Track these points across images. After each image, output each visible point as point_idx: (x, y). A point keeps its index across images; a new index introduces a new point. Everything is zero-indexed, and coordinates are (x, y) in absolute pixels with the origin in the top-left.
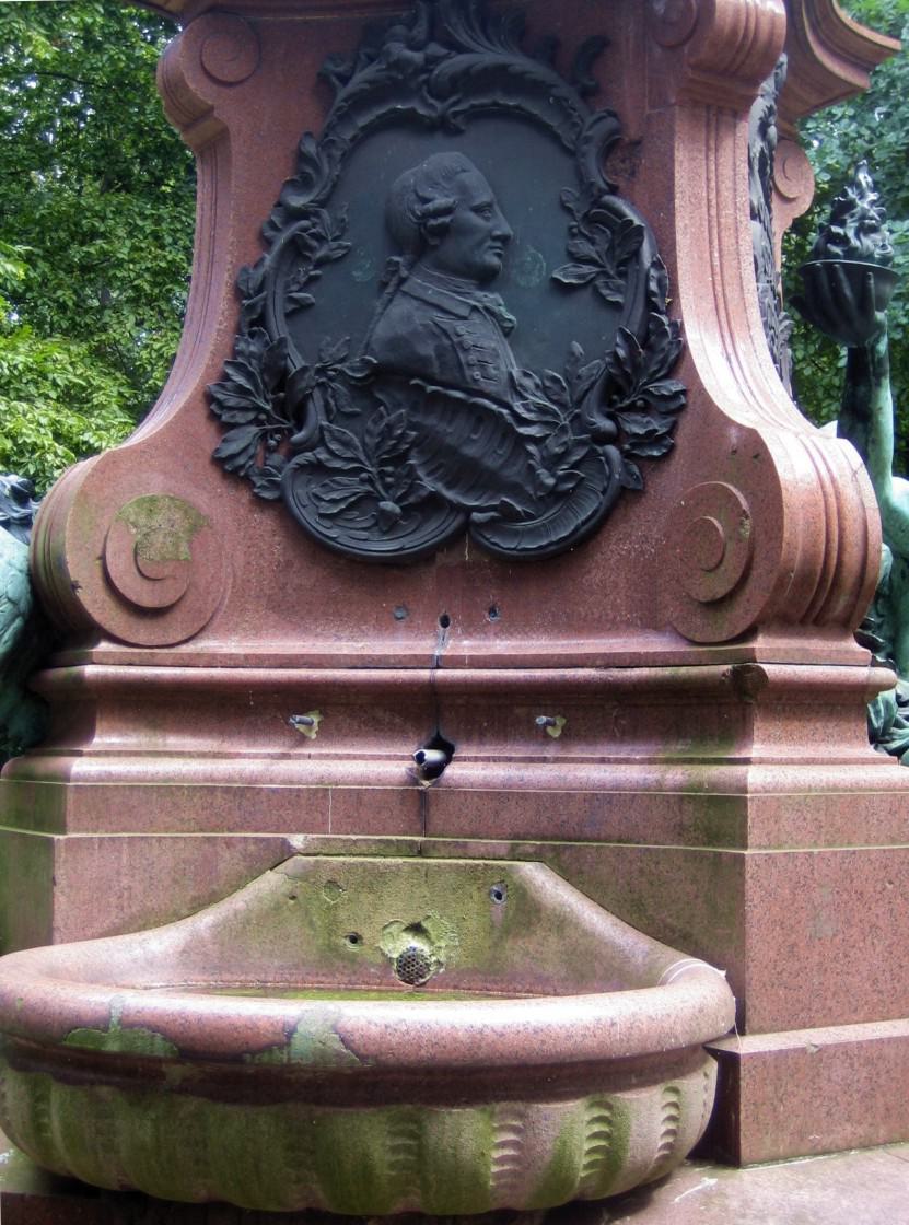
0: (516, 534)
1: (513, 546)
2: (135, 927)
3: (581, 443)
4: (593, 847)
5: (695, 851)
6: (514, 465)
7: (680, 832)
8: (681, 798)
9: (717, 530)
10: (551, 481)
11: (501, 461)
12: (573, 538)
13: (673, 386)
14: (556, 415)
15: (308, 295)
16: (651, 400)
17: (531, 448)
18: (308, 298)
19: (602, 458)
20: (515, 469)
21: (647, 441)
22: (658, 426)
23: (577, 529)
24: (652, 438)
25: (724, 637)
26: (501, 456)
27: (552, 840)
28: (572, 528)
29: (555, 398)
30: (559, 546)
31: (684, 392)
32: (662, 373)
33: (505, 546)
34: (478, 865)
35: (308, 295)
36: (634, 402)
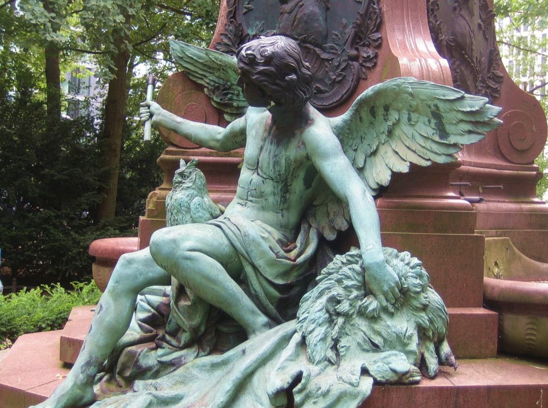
0: (322, 99)
1: (320, 104)
2: (534, 280)
3: (344, 61)
4: (415, 211)
5: (543, 232)
6: (321, 71)
7: (530, 225)
8: (531, 214)
9: (517, 123)
10: (334, 77)
11: (316, 69)
12: (342, 100)
13: (377, 35)
14: (336, 50)
15: (251, 6)
16: (371, 42)
17: (326, 64)
18: (251, 7)
19: (352, 67)
20: (321, 72)
21: (367, 60)
22: (371, 52)
23: (342, 96)
24: (368, 59)
25: (525, 162)
26: (316, 67)
27: (506, 229)
28: (340, 96)
29: (336, 42)
30: (337, 103)
31: (380, 38)
32: (375, 29)
33: (327, 104)
34: (453, 232)
35: (251, 6)
36: (365, 43)
